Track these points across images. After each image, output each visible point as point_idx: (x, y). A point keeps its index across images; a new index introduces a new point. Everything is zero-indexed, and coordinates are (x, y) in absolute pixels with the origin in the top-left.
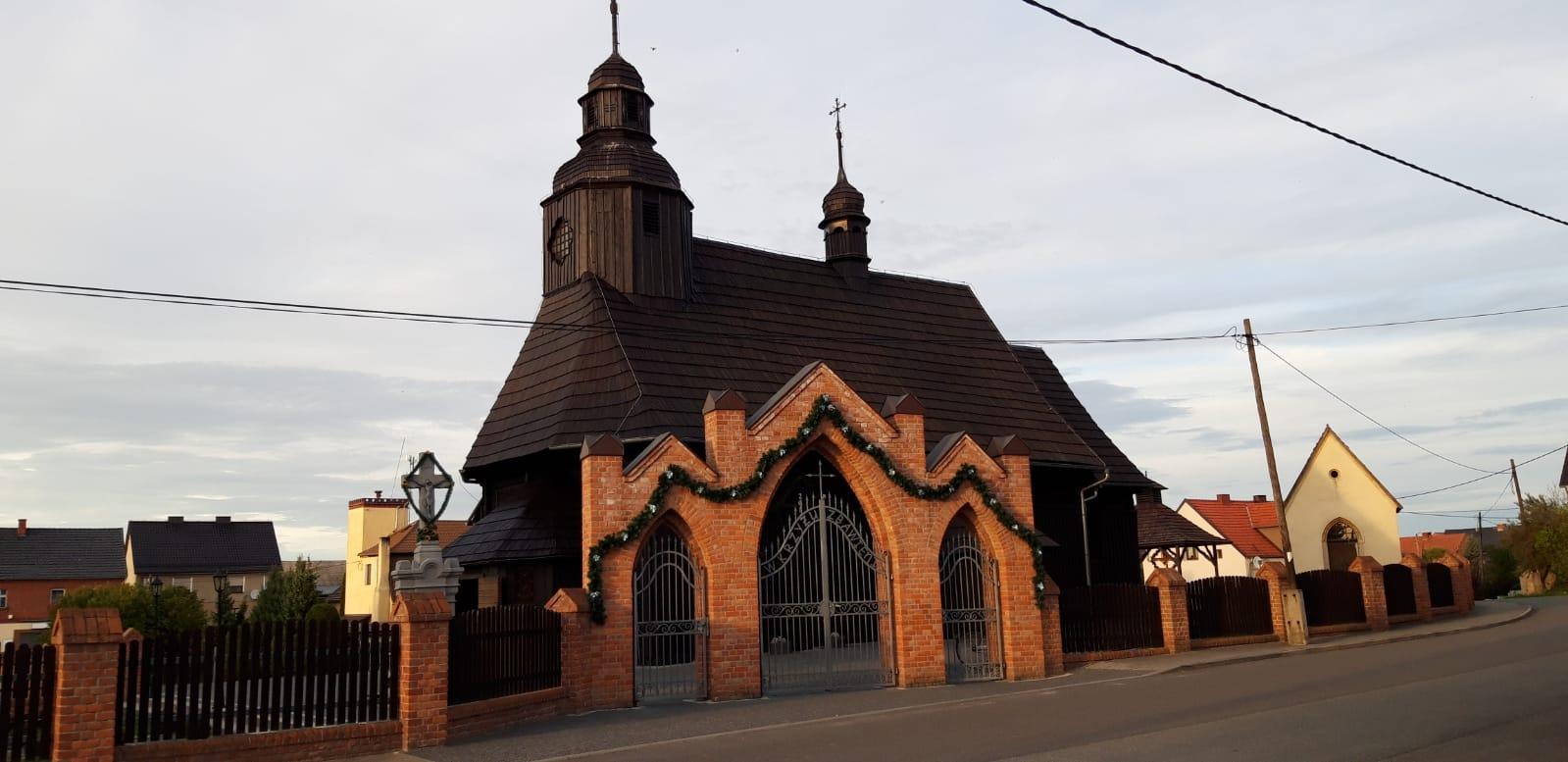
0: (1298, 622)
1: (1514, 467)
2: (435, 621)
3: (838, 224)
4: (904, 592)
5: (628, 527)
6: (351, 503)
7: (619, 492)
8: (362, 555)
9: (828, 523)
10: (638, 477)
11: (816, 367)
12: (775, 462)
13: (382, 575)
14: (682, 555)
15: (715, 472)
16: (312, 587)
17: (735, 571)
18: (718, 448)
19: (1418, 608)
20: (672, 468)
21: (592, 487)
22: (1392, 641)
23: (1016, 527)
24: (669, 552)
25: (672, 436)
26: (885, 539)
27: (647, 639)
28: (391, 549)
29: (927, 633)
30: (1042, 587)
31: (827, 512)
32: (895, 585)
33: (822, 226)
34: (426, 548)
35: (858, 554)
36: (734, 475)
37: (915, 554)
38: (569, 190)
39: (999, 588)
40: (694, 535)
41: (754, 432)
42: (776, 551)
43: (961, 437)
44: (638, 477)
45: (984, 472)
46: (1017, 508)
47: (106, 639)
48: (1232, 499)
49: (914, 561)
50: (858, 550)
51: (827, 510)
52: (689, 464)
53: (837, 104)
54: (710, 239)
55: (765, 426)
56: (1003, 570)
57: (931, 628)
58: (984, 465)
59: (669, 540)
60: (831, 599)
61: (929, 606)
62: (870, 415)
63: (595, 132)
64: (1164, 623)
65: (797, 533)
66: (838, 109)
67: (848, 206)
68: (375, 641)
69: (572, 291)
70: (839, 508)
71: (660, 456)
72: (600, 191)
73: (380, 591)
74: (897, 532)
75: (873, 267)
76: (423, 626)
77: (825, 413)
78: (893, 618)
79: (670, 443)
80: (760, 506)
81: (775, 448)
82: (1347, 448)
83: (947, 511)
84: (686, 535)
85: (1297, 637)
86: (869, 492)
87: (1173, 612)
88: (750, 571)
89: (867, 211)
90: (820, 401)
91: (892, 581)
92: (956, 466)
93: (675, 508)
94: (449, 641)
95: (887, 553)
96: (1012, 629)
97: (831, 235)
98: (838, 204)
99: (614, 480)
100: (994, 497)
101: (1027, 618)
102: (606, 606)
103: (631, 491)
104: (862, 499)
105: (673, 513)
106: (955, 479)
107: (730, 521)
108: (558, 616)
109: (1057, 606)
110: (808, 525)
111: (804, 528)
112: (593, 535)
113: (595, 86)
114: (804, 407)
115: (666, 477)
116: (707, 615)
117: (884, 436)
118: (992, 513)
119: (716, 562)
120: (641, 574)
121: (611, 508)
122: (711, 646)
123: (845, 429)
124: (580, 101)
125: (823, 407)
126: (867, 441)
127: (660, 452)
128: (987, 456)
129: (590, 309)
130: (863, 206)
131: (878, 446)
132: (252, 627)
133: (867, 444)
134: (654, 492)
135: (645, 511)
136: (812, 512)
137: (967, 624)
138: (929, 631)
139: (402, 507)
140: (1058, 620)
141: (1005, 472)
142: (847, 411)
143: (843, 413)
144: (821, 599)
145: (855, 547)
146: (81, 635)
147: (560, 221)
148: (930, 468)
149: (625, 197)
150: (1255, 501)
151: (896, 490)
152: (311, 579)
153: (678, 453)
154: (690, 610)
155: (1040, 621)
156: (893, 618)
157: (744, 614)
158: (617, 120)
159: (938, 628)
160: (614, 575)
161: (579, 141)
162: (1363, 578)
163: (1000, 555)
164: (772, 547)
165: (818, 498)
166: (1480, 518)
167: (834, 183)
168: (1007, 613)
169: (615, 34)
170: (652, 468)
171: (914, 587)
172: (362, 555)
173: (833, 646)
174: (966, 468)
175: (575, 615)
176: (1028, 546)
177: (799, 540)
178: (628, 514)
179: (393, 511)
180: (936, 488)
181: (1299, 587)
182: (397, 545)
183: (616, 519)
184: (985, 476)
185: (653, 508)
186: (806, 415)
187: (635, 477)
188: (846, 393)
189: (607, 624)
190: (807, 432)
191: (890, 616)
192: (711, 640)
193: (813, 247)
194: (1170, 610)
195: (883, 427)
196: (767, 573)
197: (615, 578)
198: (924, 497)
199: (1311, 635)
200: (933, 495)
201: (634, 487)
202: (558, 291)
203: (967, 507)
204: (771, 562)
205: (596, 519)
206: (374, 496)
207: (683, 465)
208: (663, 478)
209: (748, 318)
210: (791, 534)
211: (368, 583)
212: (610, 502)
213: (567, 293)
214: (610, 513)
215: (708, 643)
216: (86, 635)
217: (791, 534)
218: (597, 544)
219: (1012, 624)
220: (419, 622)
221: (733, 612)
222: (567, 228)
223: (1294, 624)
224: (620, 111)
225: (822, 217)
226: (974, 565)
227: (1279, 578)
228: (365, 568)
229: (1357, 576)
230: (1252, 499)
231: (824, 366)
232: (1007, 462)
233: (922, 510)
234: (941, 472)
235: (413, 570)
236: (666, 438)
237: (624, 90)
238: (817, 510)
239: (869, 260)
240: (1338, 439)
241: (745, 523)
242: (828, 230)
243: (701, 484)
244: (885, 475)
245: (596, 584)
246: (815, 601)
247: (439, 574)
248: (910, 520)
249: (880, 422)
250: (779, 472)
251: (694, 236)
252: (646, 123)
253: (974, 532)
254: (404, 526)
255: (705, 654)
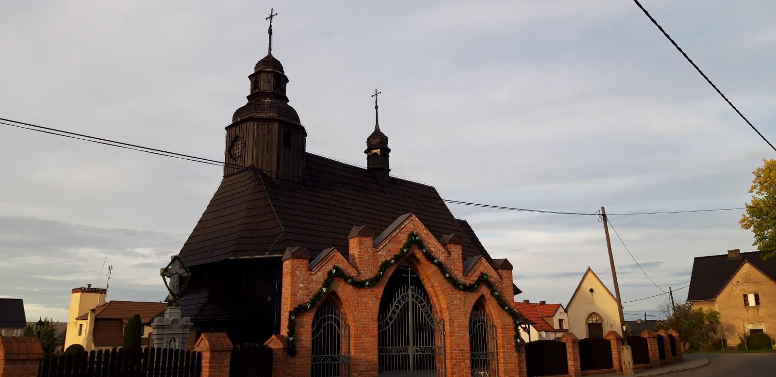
0: (629, 362)
1: (671, 291)
2: (225, 351)
3: (375, 151)
4: (451, 342)
5: (311, 300)
6: (73, 290)
7: (306, 280)
8: (77, 319)
9: (413, 302)
10: (317, 272)
11: (410, 216)
12: (389, 267)
13: (89, 330)
14: (337, 317)
15: (357, 271)
16: (52, 336)
17: (366, 327)
18: (359, 258)
19: (667, 357)
20: (335, 267)
21: (292, 276)
22: (670, 373)
23: (507, 308)
24: (330, 315)
25: (335, 250)
26: (441, 312)
27: (316, 365)
28: (96, 316)
29: (463, 365)
30: (519, 341)
31: (413, 296)
32: (446, 337)
33: (366, 152)
34: (173, 311)
35: (427, 320)
36: (367, 274)
37: (458, 321)
38: (242, 121)
39: (497, 340)
40: (343, 306)
41: (378, 250)
42: (386, 317)
43: (480, 258)
44: (317, 272)
45: (491, 278)
46: (506, 298)
47: (32, 357)
48: (530, 302)
49: (458, 325)
50: (428, 318)
51: (412, 295)
52: (343, 266)
53: (376, 92)
54: (312, 153)
55: (384, 246)
56: (499, 331)
57: (465, 362)
58: (491, 274)
59: (327, 308)
60: (414, 344)
61: (464, 350)
62: (436, 243)
63: (258, 93)
64: (569, 361)
65: (397, 307)
66: (376, 94)
67: (381, 142)
68: (99, 367)
69: (242, 174)
70: (418, 294)
71: (329, 260)
72: (261, 123)
73: (87, 339)
74: (448, 308)
75: (392, 174)
76: (216, 354)
77: (414, 241)
78: (445, 356)
79: (335, 253)
80: (379, 291)
81: (388, 259)
82: (598, 278)
83: (473, 298)
84: (339, 306)
85: (629, 370)
86: (434, 286)
87: (574, 356)
88: (374, 327)
89: (389, 146)
90: (412, 235)
91: (444, 335)
92: (477, 273)
93: (336, 290)
94: (231, 364)
95: (442, 320)
96: (504, 363)
97: (371, 156)
98: (376, 141)
99: (303, 273)
100: (496, 291)
101: (511, 358)
102: (297, 345)
103: (312, 280)
104: (429, 289)
105: (334, 294)
106: (478, 280)
107: (364, 299)
108: (271, 350)
109: (525, 351)
110: (403, 303)
111: (400, 304)
112: (291, 304)
113: (259, 69)
114: (403, 238)
115: (332, 272)
116: (349, 352)
117: (443, 256)
118: (495, 300)
119: (357, 322)
120: (315, 328)
121: (301, 289)
122: (351, 370)
123: (424, 250)
124: (250, 77)
125: (414, 238)
126: (435, 257)
127: (328, 259)
128: (492, 269)
129: (253, 184)
130: (387, 143)
131: (440, 260)
132: (89, 355)
133: (435, 259)
134: (325, 281)
135: (320, 291)
136: (405, 295)
137: (481, 360)
138: (463, 364)
139: (102, 293)
140: (525, 359)
141: (501, 278)
142: (425, 241)
143: (423, 242)
144: (408, 344)
145: (426, 316)
146: (16, 354)
147: (236, 138)
148: (465, 274)
149: (274, 128)
150: (540, 304)
151: (448, 285)
152: (52, 331)
153: (338, 259)
154: (337, 348)
155: (517, 359)
156: (445, 356)
157: (370, 352)
158: (271, 87)
159: (468, 362)
160: (302, 328)
161: (248, 97)
162: (648, 341)
163: (497, 322)
164: (384, 315)
165: (408, 288)
166: (645, 315)
167: (373, 131)
168: (501, 355)
169: (270, 44)
170: (324, 267)
171: (456, 339)
172: (77, 319)
173: (414, 368)
174: (482, 275)
175: (282, 350)
176: (511, 318)
177: (398, 311)
178: (310, 292)
179: (98, 295)
180: (468, 285)
181: (629, 344)
182: (99, 314)
183: (304, 295)
184: (491, 280)
185: (325, 290)
186: (404, 241)
187: (315, 272)
188: (424, 231)
189: (296, 357)
190: (405, 251)
191: (443, 355)
192: (351, 367)
193: (361, 161)
194: (572, 354)
195: (442, 250)
196: (382, 329)
197: (302, 329)
198: (462, 290)
199: (635, 368)
200: (468, 289)
201: (314, 277)
202: (232, 175)
203: (483, 296)
204: (383, 323)
205: (293, 295)
206: (87, 286)
207: (341, 266)
208: (330, 273)
209: (333, 195)
210: (394, 308)
211: (80, 334)
212: (301, 285)
213: (238, 175)
214: (301, 292)
215: (349, 368)
216: (20, 354)
217: (394, 308)
218: (292, 309)
219: (504, 360)
220: (214, 351)
221: (364, 351)
222: (240, 141)
223: (627, 363)
224: (273, 83)
225: (366, 148)
226: (485, 328)
227: (573, 342)
228: (78, 326)
229: (645, 339)
230: (523, 302)
231: (414, 216)
232: (501, 273)
233: (461, 296)
234: (471, 276)
235: (165, 323)
236: (333, 250)
237: (274, 72)
238: (408, 294)
239: (390, 170)
240: (594, 274)
241: (372, 299)
242: (369, 154)
243: (350, 277)
244: (443, 277)
245: (292, 332)
246: (405, 345)
247: (179, 326)
248: (455, 302)
249: (441, 248)
250: (390, 273)
251: (306, 151)
252: (284, 90)
253: (484, 310)
254: (102, 304)
255: (347, 375)
